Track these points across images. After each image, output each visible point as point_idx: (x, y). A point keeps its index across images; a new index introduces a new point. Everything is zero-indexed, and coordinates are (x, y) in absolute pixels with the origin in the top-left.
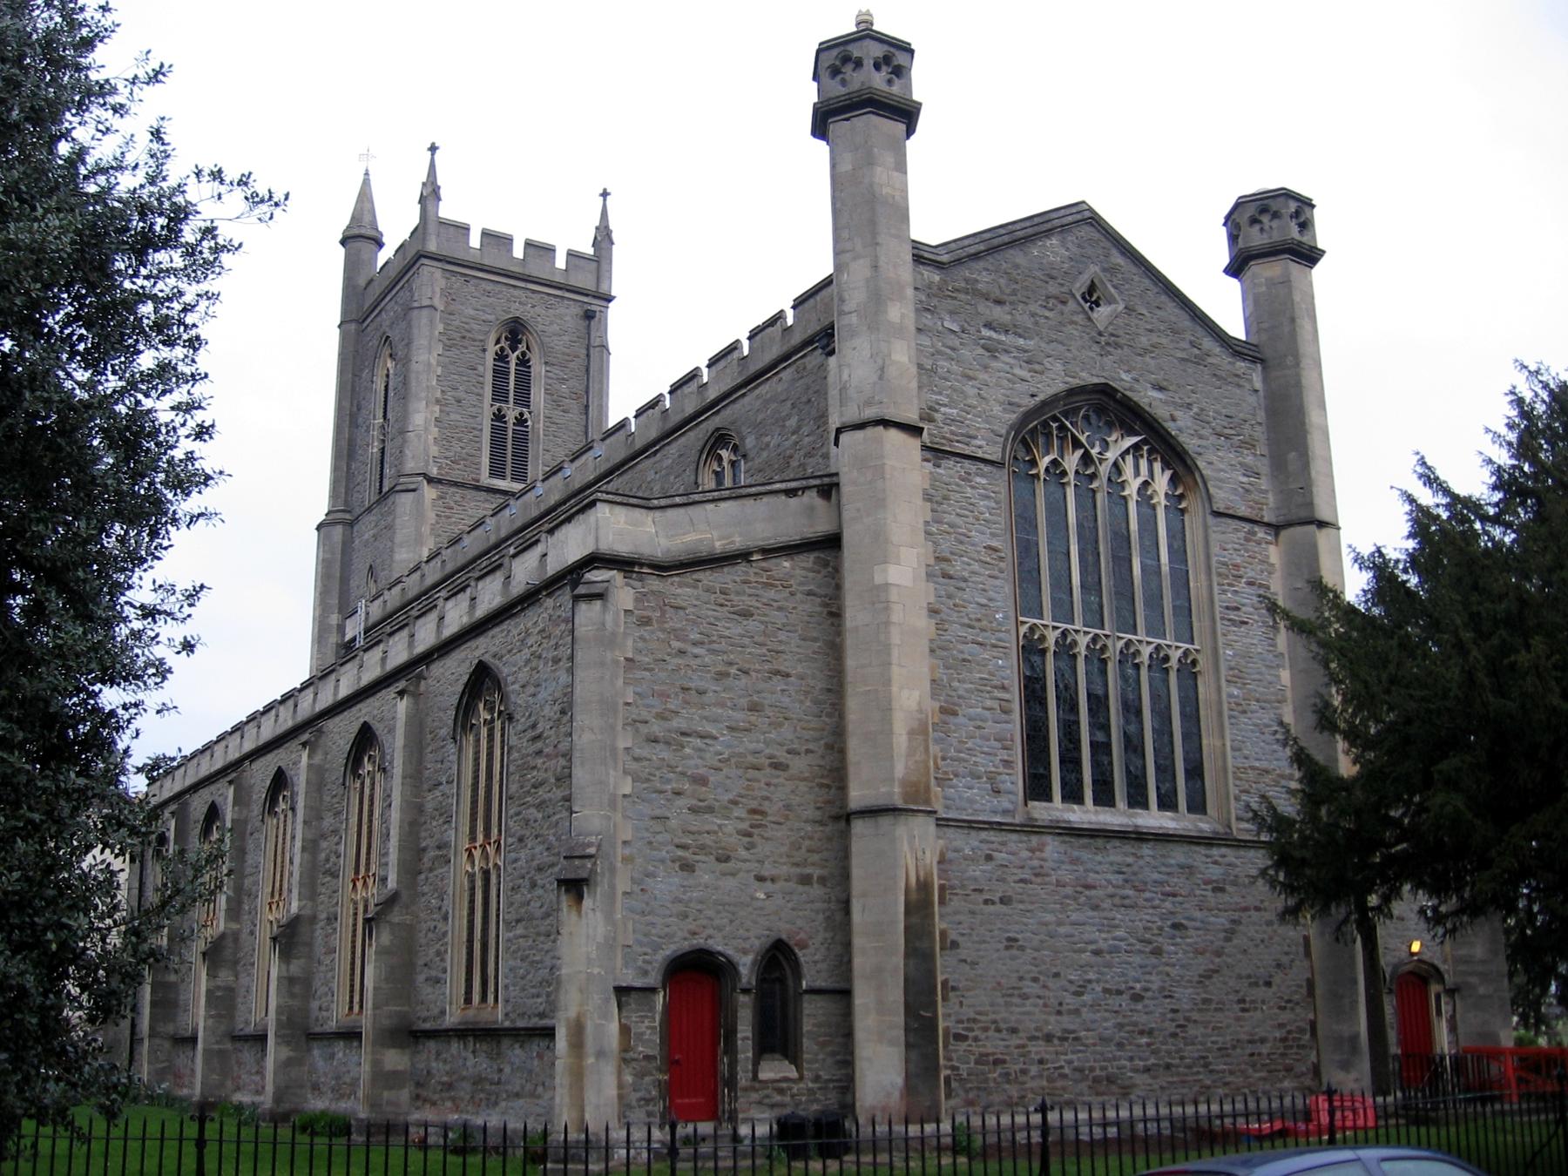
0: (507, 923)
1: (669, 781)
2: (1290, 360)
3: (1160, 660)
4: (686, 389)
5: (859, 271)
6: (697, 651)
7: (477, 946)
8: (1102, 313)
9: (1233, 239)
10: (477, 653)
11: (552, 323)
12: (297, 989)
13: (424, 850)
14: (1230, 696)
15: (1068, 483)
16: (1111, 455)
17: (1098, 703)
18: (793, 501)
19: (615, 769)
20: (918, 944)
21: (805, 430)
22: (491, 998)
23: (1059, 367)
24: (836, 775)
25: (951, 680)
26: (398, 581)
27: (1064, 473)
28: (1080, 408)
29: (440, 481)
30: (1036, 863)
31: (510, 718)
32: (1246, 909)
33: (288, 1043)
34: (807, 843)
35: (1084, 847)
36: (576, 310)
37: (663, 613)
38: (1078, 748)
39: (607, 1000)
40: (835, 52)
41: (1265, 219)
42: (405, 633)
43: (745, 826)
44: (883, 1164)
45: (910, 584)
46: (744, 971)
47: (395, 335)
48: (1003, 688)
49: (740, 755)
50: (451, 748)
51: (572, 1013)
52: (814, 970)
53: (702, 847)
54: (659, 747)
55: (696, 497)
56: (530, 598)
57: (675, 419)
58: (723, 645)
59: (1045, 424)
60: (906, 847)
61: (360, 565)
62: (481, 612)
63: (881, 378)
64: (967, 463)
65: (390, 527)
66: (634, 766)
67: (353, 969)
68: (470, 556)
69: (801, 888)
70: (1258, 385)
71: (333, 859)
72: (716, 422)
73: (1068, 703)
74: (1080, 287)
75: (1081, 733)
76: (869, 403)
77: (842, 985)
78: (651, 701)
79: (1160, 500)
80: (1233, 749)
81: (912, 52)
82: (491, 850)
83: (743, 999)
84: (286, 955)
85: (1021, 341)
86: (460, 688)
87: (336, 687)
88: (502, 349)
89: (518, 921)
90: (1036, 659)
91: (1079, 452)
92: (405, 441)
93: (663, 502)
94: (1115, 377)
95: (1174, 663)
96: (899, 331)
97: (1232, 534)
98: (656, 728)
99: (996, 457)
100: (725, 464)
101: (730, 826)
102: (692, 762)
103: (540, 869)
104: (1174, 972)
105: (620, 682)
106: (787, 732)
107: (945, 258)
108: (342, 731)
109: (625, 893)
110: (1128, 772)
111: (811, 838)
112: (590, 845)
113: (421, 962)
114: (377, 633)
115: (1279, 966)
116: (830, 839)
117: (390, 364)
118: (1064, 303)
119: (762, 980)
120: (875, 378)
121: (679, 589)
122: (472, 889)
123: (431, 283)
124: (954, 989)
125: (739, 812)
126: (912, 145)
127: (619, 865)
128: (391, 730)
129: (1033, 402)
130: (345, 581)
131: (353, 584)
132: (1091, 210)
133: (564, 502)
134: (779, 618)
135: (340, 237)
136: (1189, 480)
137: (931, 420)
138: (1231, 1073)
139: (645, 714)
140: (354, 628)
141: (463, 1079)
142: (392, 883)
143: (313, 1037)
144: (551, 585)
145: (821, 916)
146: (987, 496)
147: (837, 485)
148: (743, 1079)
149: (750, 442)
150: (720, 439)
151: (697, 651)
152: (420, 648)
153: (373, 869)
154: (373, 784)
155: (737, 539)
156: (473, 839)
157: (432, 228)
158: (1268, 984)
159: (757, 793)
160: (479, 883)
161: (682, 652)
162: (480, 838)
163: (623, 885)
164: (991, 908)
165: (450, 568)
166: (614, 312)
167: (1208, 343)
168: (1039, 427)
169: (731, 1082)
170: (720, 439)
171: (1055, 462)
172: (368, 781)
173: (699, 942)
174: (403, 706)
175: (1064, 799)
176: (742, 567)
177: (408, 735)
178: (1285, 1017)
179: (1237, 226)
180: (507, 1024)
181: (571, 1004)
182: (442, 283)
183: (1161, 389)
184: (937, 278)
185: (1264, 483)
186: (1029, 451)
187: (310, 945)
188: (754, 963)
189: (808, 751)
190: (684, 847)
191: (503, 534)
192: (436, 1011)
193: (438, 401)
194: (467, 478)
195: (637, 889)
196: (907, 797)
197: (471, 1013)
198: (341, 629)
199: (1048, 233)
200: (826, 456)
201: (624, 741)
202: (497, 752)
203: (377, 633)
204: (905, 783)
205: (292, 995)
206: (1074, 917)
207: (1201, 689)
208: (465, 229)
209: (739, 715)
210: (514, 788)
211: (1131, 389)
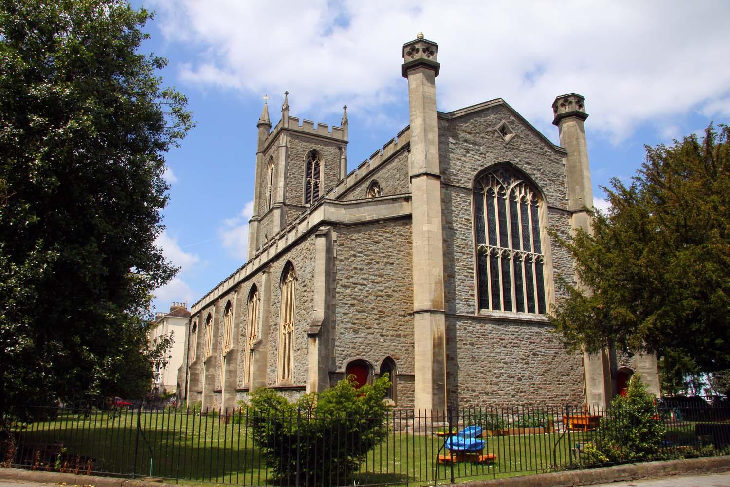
3: (528, 260)
8: (508, 138)
9: (556, 111)
10: (287, 258)
15: (495, 197)
19: (330, 296)
20: (438, 358)
30: (482, 330)
31: (297, 279)
33: (229, 393)
42: (266, 252)
44: (417, 436)
45: (436, 231)
48: (472, 269)
62: (289, 243)
63: (426, 158)
65: (272, 221)
79: (529, 202)
81: (437, 46)
82: (291, 325)
88: (310, 160)
89: (298, 350)
95: (534, 260)
96: (432, 143)
100: (376, 192)
115: (572, 369)
117: (273, 166)
123: (283, 140)
124: (452, 375)
125: (375, 312)
132: (503, 101)
135: (257, 124)
137: (445, 174)
147: (411, 197)
152: (270, 257)
155: (375, 216)
156: (286, 322)
157: (286, 120)
158: (568, 375)
160: (287, 337)
164: (466, 347)
171: (490, 189)
172: (255, 303)
173: (364, 358)
174: (264, 276)
175: (493, 308)
177: (266, 287)
180: (295, 385)
184: (447, 125)
187: (236, 359)
190: (354, 324)
192: (273, 381)
194: (299, 204)
200: (408, 188)
205: (231, 376)
206: (497, 350)
211: (517, 164)
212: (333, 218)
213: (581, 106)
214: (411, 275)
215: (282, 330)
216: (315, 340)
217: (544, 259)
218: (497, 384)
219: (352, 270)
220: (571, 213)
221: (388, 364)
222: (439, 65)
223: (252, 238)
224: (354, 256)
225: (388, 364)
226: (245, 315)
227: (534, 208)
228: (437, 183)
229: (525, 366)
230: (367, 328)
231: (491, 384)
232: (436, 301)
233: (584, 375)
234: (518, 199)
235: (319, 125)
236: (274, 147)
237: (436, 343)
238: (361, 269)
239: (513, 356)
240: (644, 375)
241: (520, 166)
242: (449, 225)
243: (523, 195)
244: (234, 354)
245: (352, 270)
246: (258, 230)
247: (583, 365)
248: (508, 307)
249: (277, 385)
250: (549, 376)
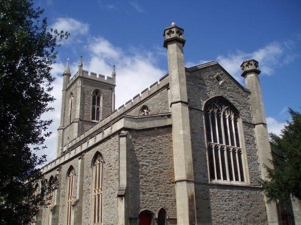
7: (97, 210)
8: (221, 83)
10: (96, 150)
12: (56, 221)
16: (223, 110)
21: (163, 104)
22: (100, 221)
31: (104, 162)
56: (109, 138)
57: (134, 104)
58: (149, 147)
61: (66, 137)
62: (97, 141)
64: (197, 111)
71: (64, 193)
72: (143, 104)
84: (54, 214)
86: (93, 157)
87: (65, 158)
107: (190, 71)
109: (131, 198)
114: (70, 150)
117: (72, 98)
122: (96, 198)
127: (129, 192)
128: (77, 166)
144: (113, 135)
150: (145, 107)
152: (83, 150)
156: (95, 188)
158: (259, 217)
160: (97, 197)
162: (97, 188)
166: (116, 88)
173: (148, 209)
177: (81, 165)
198: (62, 149)
202: (101, 170)
203: (70, 150)
205: (55, 222)
206: (221, 203)
212: (129, 127)
213: (257, 66)
214: (172, 160)
215: (93, 193)
216: (122, 199)
217: (242, 150)
219: (140, 157)
221: (162, 212)
223: (59, 139)
224: (141, 148)
225: (162, 212)
227: (235, 122)
229: (236, 212)
230: (150, 191)
232: (190, 175)
233: (267, 216)
234: (227, 117)
236: (73, 87)
237: (190, 198)
238: (146, 156)
239: (230, 206)
241: (227, 98)
244: (57, 208)
245: (140, 157)
246: (63, 135)
247: (266, 210)
248: (225, 178)
250: (249, 218)
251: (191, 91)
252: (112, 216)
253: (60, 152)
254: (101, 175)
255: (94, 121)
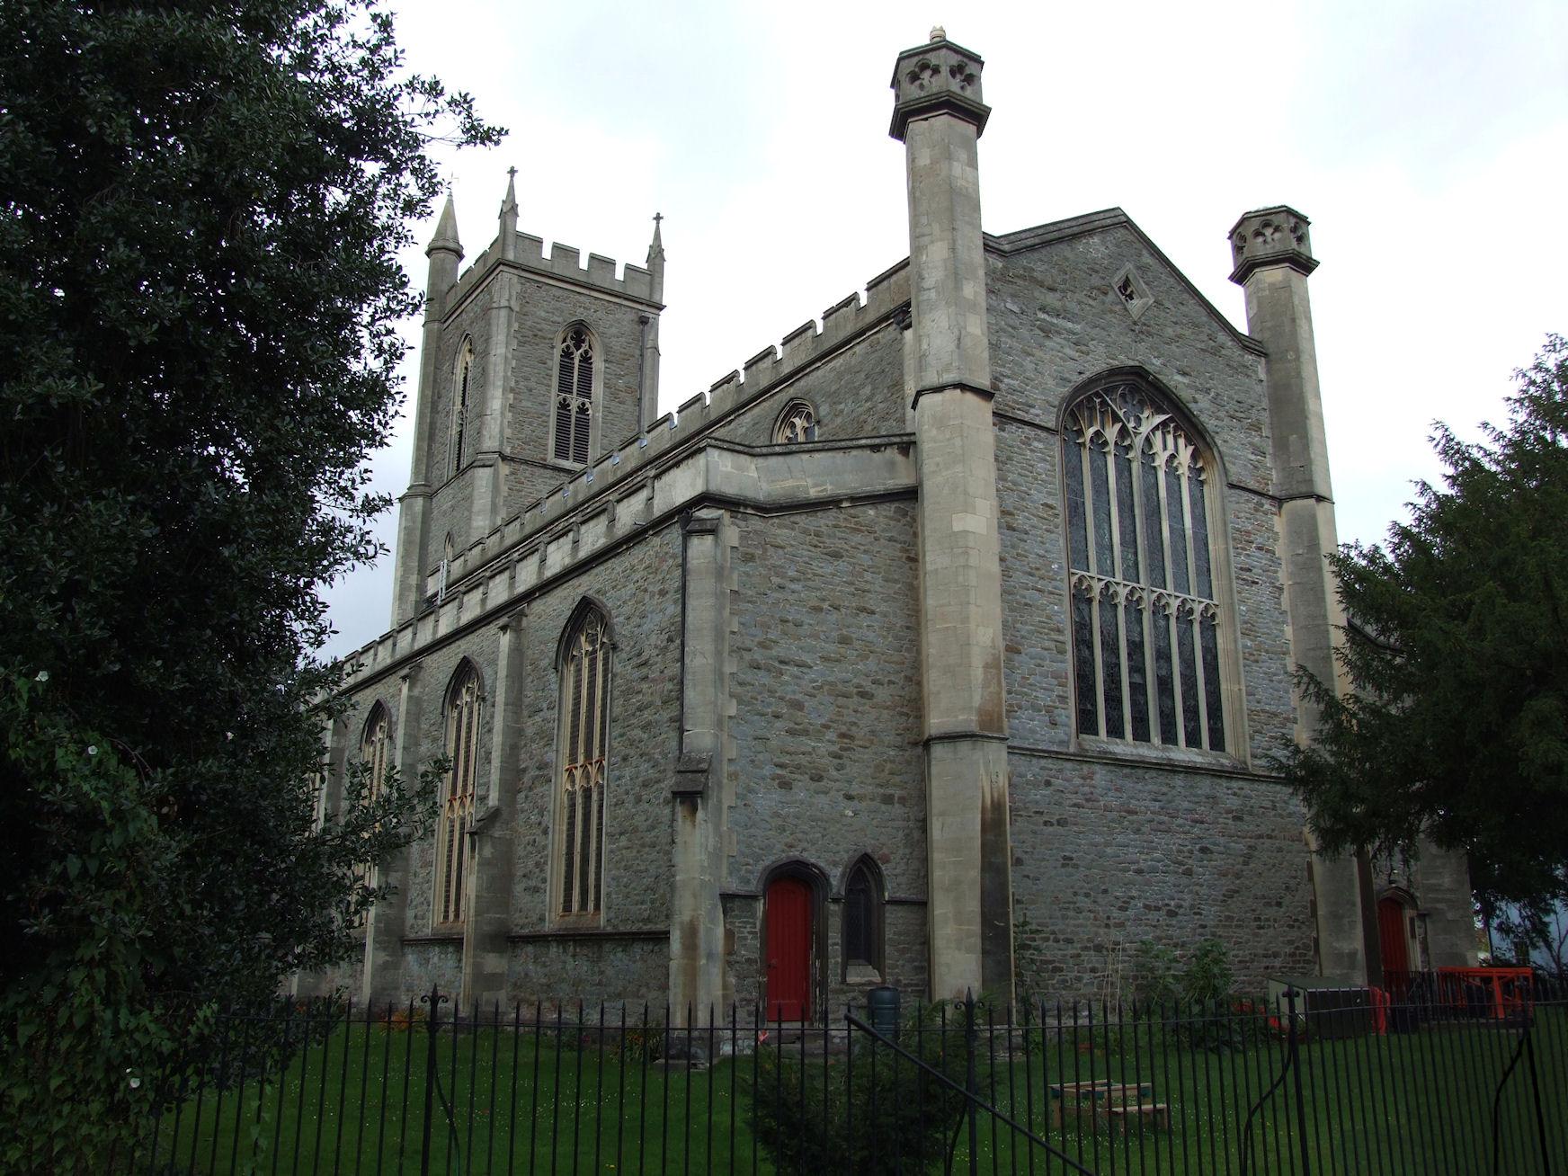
0: (610, 835)
1: (769, 705)
2: (1291, 356)
3: (1185, 614)
4: (761, 365)
5: (937, 252)
6: (793, 586)
8: (1136, 305)
9: (1238, 249)
10: (581, 591)
11: (610, 326)
13: (524, 770)
14: (1245, 646)
16: (1145, 429)
17: (1136, 648)
18: (876, 456)
21: (879, 398)
22: (591, 906)
23: (1101, 349)
24: (915, 706)
25: (1015, 621)
26: (479, 543)
27: (1106, 443)
28: (1117, 387)
29: (512, 460)
30: (1086, 789)
31: (615, 647)
32: (1260, 837)
33: (385, 949)
34: (889, 766)
35: (1126, 776)
36: (632, 316)
37: (765, 551)
38: (1119, 689)
39: (715, 906)
40: (915, 59)
41: (1268, 232)
43: (835, 748)
46: (834, 882)
47: (475, 331)
48: (1059, 631)
49: (831, 684)
50: (553, 677)
51: (686, 917)
52: (895, 883)
53: (798, 767)
54: (761, 673)
55: (794, 448)
56: (637, 536)
59: (1090, 399)
60: (982, 771)
61: (438, 531)
62: (583, 553)
63: (958, 346)
64: (1027, 429)
66: (739, 690)
67: (448, 882)
68: (549, 518)
69: (884, 807)
70: (1263, 376)
72: (791, 392)
73: (1111, 647)
74: (1117, 280)
75: (1125, 678)
76: (947, 369)
77: (921, 897)
78: (753, 631)
79: (1184, 471)
80: (1249, 694)
81: (982, 63)
82: (593, 770)
83: (833, 907)
85: (1070, 325)
87: (436, 626)
90: (1083, 606)
91: (1118, 426)
92: (482, 423)
93: (764, 450)
94: (1147, 358)
95: (1196, 616)
96: (973, 307)
97: (1246, 503)
98: (758, 655)
99: (1051, 425)
100: (798, 429)
101: (823, 748)
102: (789, 688)
103: (645, 785)
104: (1204, 891)
105: (727, 612)
106: (872, 664)
107: (1007, 247)
108: (441, 667)
110: (1162, 712)
111: (893, 762)
112: (703, 760)
113: (520, 873)
116: (909, 763)
117: (469, 358)
118: (1106, 294)
119: (849, 891)
120: (952, 346)
121: (779, 530)
123: (506, 287)
125: (831, 735)
126: (982, 144)
128: (493, 662)
129: (1080, 379)
130: (423, 546)
131: (432, 548)
133: (640, 469)
134: (865, 560)
136: (1208, 454)
138: (1250, 983)
139: (748, 643)
140: (435, 585)
141: (563, 980)
142: (493, 800)
143: (405, 943)
144: (658, 525)
145: (901, 834)
146: (1046, 455)
148: (833, 981)
149: (824, 410)
150: (794, 408)
151: (793, 586)
152: (521, 588)
153: (470, 790)
154: (471, 713)
157: (510, 240)
158: (1279, 904)
159: (846, 719)
160: (579, 800)
161: (781, 587)
162: (581, 759)
163: (728, 799)
165: (528, 530)
166: (664, 319)
167: (1222, 337)
168: (1085, 402)
169: (823, 984)
170: (794, 408)
171: (1098, 433)
172: (465, 711)
173: (795, 854)
174: (506, 640)
175: (1109, 733)
176: (833, 513)
177: (509, 665)
178: (1294, 934)
179: (1243, 238)
180: (609, 929)
181: (685, 907)
182: (518, 288)
183: (1185, 374)
185: (1269, 462)
186: (1076, 421)
188: (843, 875)
189: (890, 682)
191: (580, 498)
192: (535, 918)
193: (512, 390)
194: (537, 457)
195: (740, 803)
196: (982, 725)
197: (571, 919)
198: (421, 588)
199: (1091, 232)
201: (730, 667)
203: (471, 580)
204: (980, 712)
206: (1120, 839)
207: (1220, 640)
208: (539, 242)
209: (832, 647)
210: (617, 711)
218: (1121, 925)
220: (1279, 501)
222: (987, 111)
226: (435, 740)
228: (982, 411)
229: (1185, 880)
231: (1107, 926)
233: (1314, 904)
234: (1161, 461)
235: (593, 257)
240: (1439, 906)
242: (1008, 518)
243: (1173, 451)
248: (1142, 734)
249: (548, 927)
251: (1006, 341)
252: (647, 881)
253: (413, 597)
254: (598, 703)
255: (567, 464)
